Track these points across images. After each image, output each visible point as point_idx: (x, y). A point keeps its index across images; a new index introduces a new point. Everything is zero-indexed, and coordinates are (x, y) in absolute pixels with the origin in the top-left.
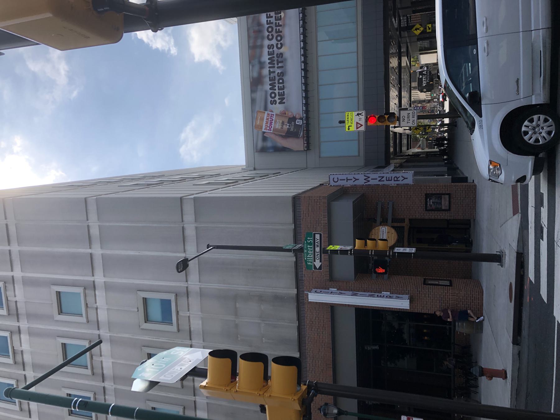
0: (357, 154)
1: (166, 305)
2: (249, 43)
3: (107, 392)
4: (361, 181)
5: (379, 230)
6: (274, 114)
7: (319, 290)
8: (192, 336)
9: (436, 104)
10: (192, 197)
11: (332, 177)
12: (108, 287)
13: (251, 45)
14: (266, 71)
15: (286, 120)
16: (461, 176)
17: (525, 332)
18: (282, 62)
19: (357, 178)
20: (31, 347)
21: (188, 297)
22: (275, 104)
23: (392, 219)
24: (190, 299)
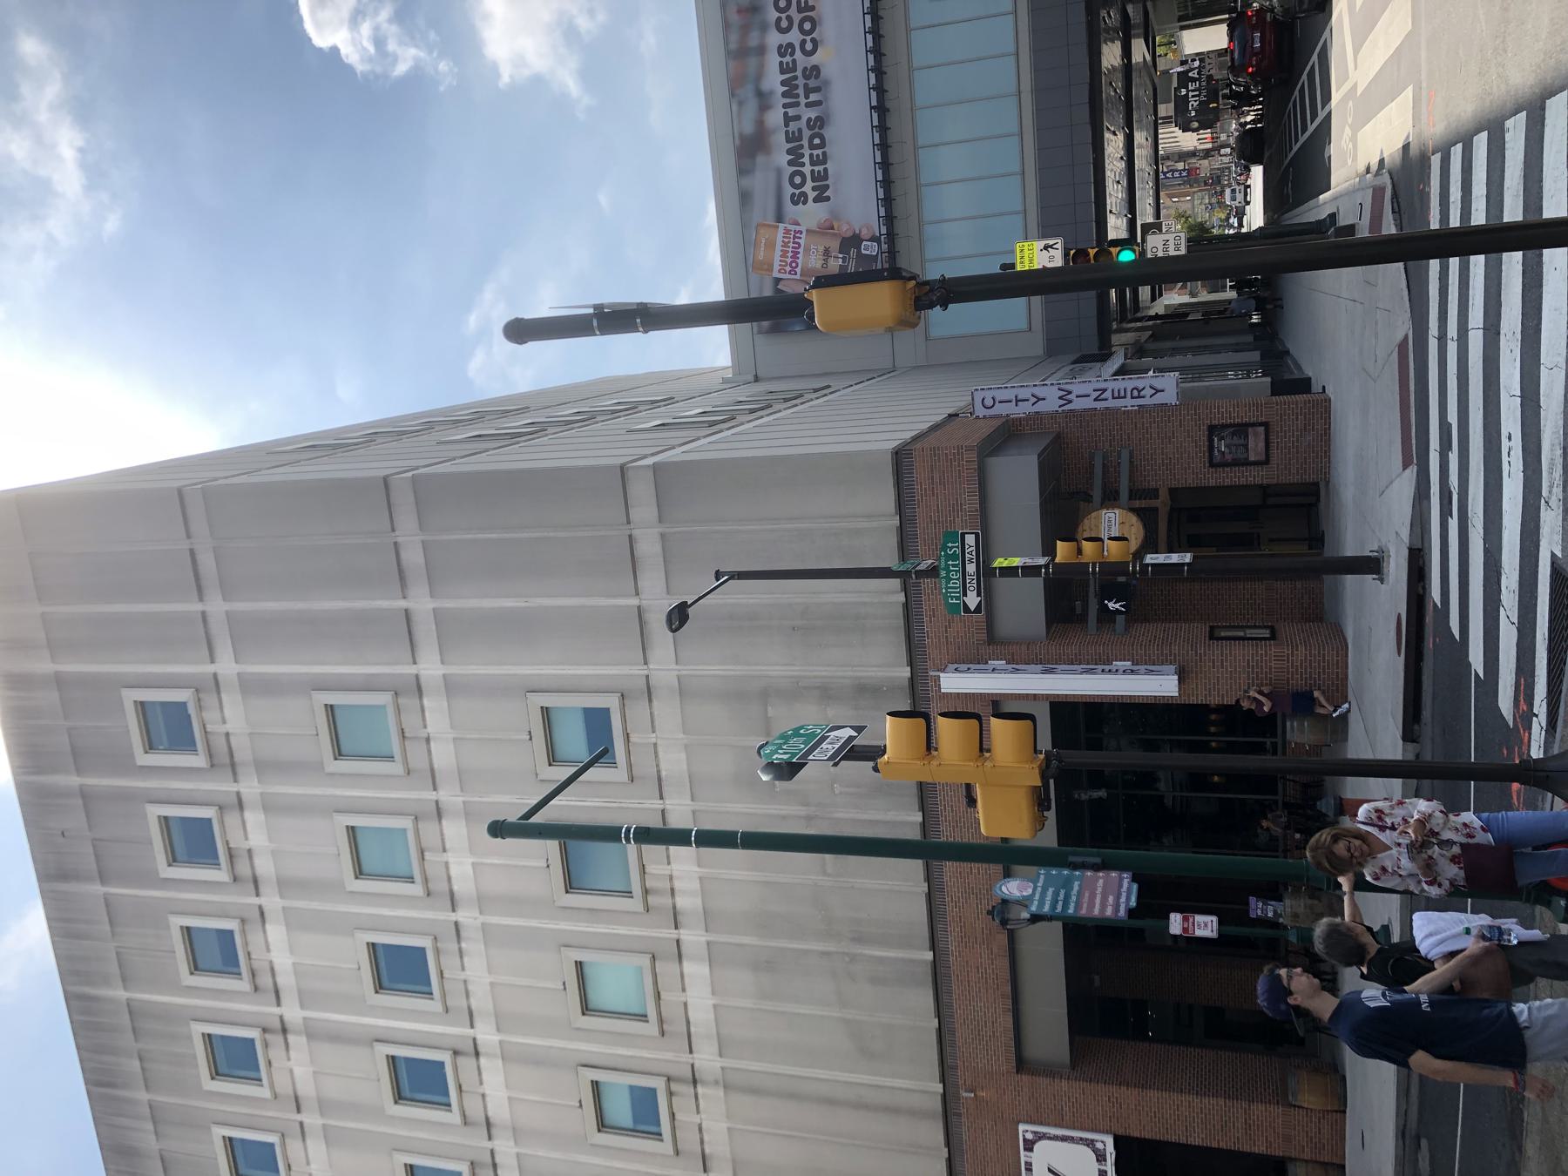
0: (1025, 326)
1: (597, 722)
2: (726, 43)
3: (463, 934)
4: (1052, 403)
5: (1098, 518)
6: (803, 229)
7: (963, 667)
8: (665, 789)
9: (1226, 159)
10: (649, 461)
11: (978, 397)
12: (451, 687)
13: (733, 46)
14: (775, 117)
15: (835, 245)
16: (1297, 375)
17: (1426, 714)
18: (817, 90)
19: (1041, 395)
20: (270, 840)
21: (650, 700)
22: (805, 203)
23: (1104, 492)
24: (655, 703)
